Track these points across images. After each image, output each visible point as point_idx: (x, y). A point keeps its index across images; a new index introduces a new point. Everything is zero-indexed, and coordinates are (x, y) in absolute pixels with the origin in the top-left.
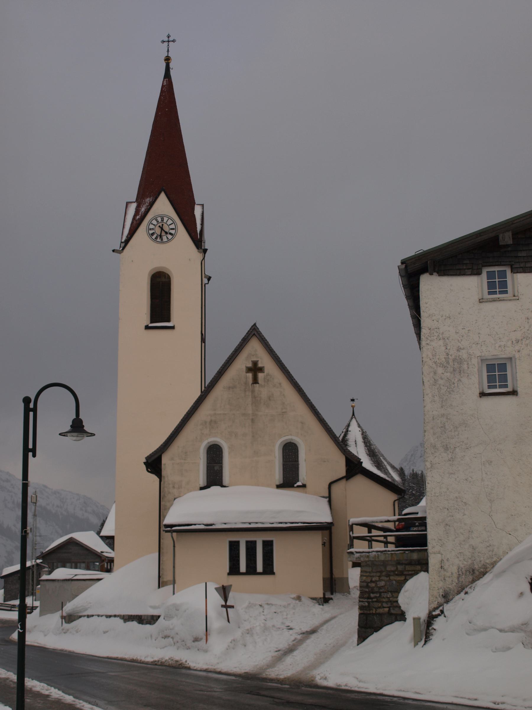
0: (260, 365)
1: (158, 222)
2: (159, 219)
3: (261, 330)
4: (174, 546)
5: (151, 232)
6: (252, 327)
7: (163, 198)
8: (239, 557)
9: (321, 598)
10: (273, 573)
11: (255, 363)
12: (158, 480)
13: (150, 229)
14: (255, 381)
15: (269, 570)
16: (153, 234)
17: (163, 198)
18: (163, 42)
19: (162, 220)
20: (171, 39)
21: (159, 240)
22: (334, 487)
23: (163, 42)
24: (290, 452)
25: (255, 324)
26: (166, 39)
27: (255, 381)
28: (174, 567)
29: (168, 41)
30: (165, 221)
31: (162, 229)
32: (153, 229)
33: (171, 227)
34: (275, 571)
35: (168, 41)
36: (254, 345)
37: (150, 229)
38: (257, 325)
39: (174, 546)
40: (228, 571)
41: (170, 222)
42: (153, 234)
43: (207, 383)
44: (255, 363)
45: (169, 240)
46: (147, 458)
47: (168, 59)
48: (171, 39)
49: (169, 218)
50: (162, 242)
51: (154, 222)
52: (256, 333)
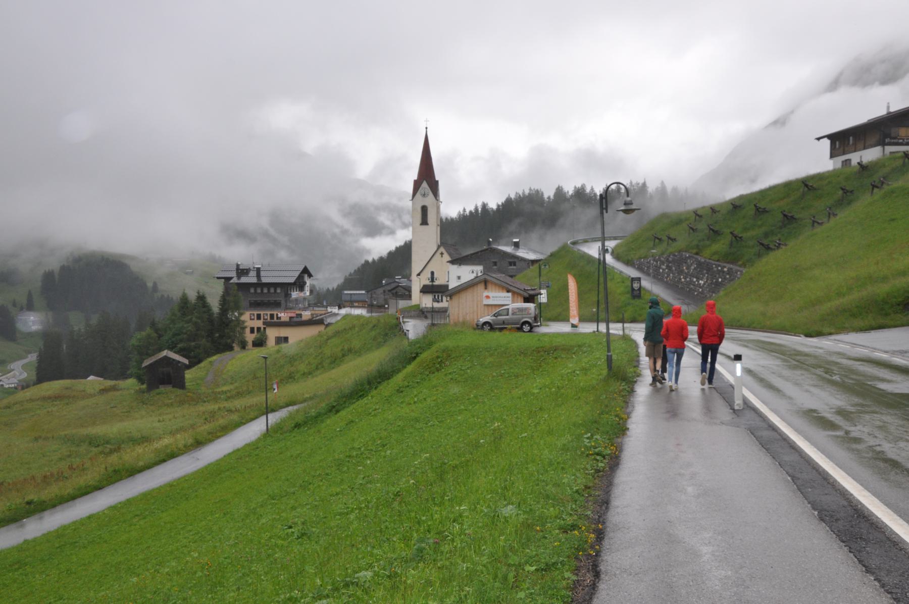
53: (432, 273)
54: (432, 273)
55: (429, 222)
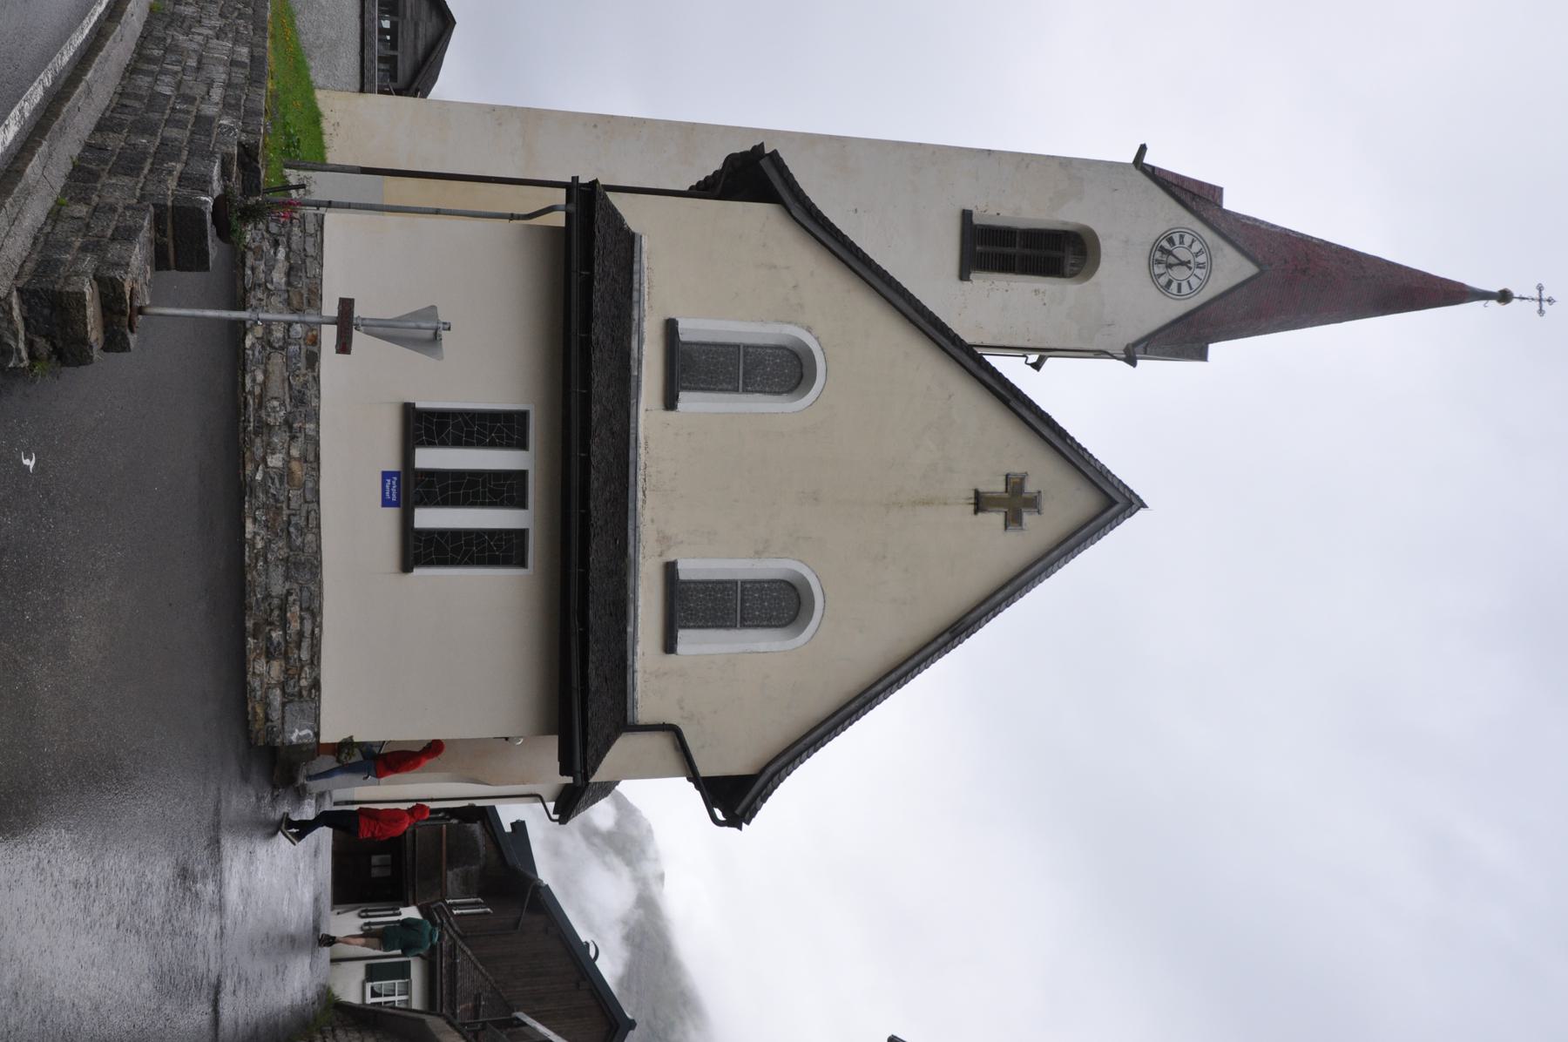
0: (1028, 518)
1: (1197, 255)
2: (1202, 259)
3: (1128, 524)
4: (512, 217)
5: (1176, 238)
6: (1137, 497)
7: (1248, 269)
8: (492, 445)
9: (317, 735)
10: (406, 568)
11: (1033, 503)
12: (686, 188)
13: (1182, 237)
14: (980, 503)
15: (421, 550)
16: (1171, 241)
17: (1248, 269)
18: (1540, 289)
19: (1199, 266)
20: (1545, 305)
21: (1158, 255)
22: (661, 742)
23: (1540, 289)
24: (780, 604)
25: (1143, 505)
26: (1545, 296)
27: (980, 503)
28: (437, 212)
29: (1540, 300)
30: (1198, 272)
31: (1182, 263)
32: (1182, 242)
33: (1185, 286)
34: (419, 572)
35: (1540, 300)
36: (1081, 502)
37: (1182, 237)
38: (1141, 512)
39: (512, 217)
40: (420, 405)
41: (1195, 282)
42: (1171, 241)
43: (987, 358)
44: (1033, 503)
45: (1155, 278)
46: (774, 156)
47: (1504, 297)
48: (1545, 305)
49: (1204, 283)
50: (1153, 262)
51: (1196, 247)
52: (1115, 509)
53: (785, 370)
54: (785, 370)
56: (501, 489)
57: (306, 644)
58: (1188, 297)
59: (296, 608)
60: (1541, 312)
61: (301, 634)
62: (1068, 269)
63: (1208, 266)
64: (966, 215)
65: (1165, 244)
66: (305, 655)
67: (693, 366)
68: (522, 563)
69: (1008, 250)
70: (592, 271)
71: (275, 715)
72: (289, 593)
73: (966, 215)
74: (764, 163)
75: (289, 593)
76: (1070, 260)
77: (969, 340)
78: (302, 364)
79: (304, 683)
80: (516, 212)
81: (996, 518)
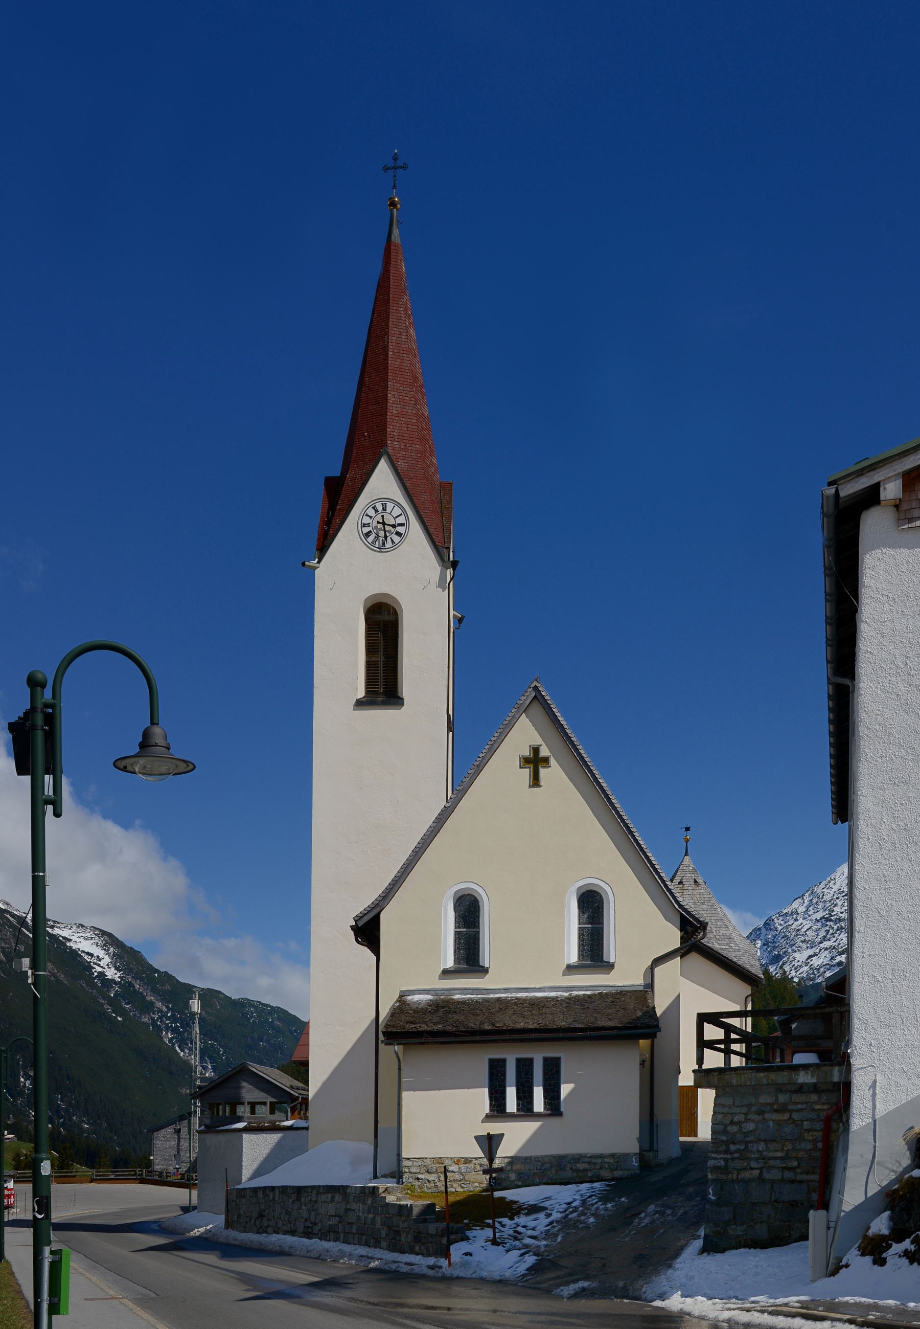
1: (377, 511)
2: (379, 507)
4: (400, 1069)
5: (366, 530)
9: (635, 1154)
14: (535, 781)
16: (368, 535)
18: (386, 169)
20: (400, 163)
23: (386, 169)
24: (591, 904)
27: (535, 781)
30: (388, 510)
34: (562, 1109)
37: (364, 525)
39: (400, 1069)
42: (368, 535)
53: (468, 911)
54: (468, 911)
55: (407, 688)
56: (525, 1067)
57: (594, 1161)
58: (407, 517)
59: (578, 1165)
60: (404, 167)
61: (589, 1163)
62: (391, 618)
63: (385, 502)
64: (360, 704)
65: (371, 539)
66: (599, 1161)
67: (469, 956)
68: (559, 1059)
69: (381, 665)
70: (423, 1032)
71: (626, 1173)
72: (571, 1169)
73: (360, 704)
74: (360, 924)
75: (571, 1169)
76: (386, 617)
77: (443, 803)
78: (469, 1166)
79: (612, 1161)
80: (397, 1067)
81: (543, 772)
